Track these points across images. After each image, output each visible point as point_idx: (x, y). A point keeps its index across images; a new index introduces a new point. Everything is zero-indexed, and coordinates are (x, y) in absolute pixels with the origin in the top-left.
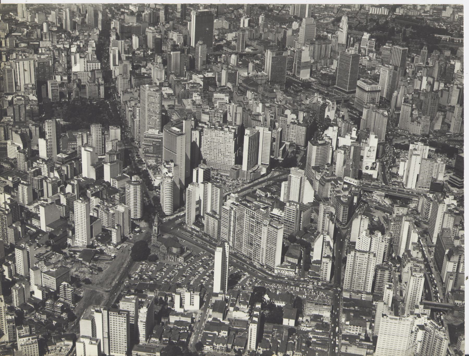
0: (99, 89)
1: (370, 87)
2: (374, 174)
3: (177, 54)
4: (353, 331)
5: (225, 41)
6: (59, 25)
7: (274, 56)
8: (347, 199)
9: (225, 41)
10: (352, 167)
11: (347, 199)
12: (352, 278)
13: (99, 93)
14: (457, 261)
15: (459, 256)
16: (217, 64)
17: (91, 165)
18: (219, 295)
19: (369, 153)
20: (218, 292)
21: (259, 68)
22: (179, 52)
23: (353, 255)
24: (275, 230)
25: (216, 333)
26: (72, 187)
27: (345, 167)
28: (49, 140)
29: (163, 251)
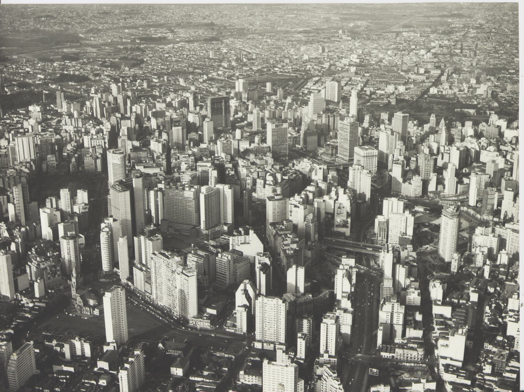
0: (96, 162)
1: (366, 152)
2: (347, 231)
3: (178, 130)
4: (249, 381)
5: (246, 122)
6: (90, 113)
7: (274, 127)
8: (292, 252)
9: (246, 122)
10: (312, 223)
11: (292, 252)
12: (263, 327)
13: (96, 166)
14: (390, 310)
15: (391, 305)
16: (221, 138)
17: (49, 226)
18: (111, 344)
19: (339, 210)
20: (110, 341)
21: (264, 140)
22: (180, 128)
23: (261, 302)
24: (187, 278)
25: (93, 382)
26: (16, 244)
27: (305, 223)
28: (17, 205)
29: (79, 304)
